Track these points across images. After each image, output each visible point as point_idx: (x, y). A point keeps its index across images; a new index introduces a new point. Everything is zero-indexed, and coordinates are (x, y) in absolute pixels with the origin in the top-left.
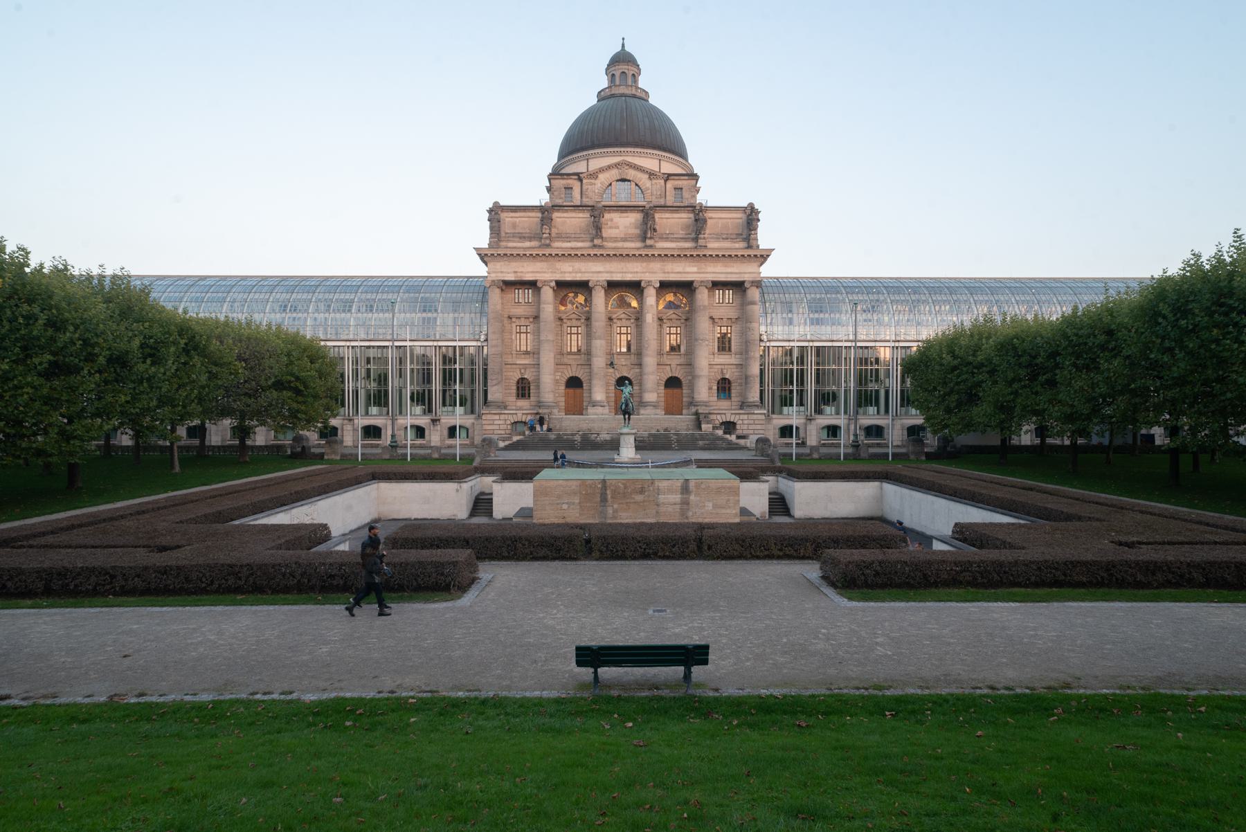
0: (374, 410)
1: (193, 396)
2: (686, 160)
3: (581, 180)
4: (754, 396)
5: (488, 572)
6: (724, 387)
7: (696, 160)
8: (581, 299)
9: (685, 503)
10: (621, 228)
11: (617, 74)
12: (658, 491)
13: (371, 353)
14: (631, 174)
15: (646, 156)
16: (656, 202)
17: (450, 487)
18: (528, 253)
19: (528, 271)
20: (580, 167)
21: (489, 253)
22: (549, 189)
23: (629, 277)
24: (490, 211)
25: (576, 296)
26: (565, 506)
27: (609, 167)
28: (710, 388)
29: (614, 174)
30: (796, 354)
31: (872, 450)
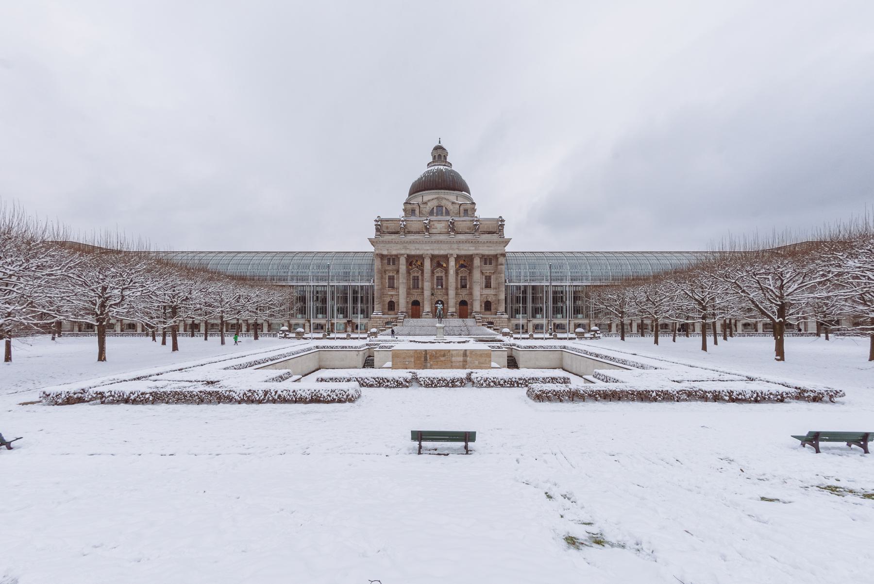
0: (320, 316)
1: (294, 335)
4: (502, 308)
6: (488, 306)
7: (474, 196)
12: (452, 356)
13: (319, 289)
22: (405, 210)
30: (522, 289)
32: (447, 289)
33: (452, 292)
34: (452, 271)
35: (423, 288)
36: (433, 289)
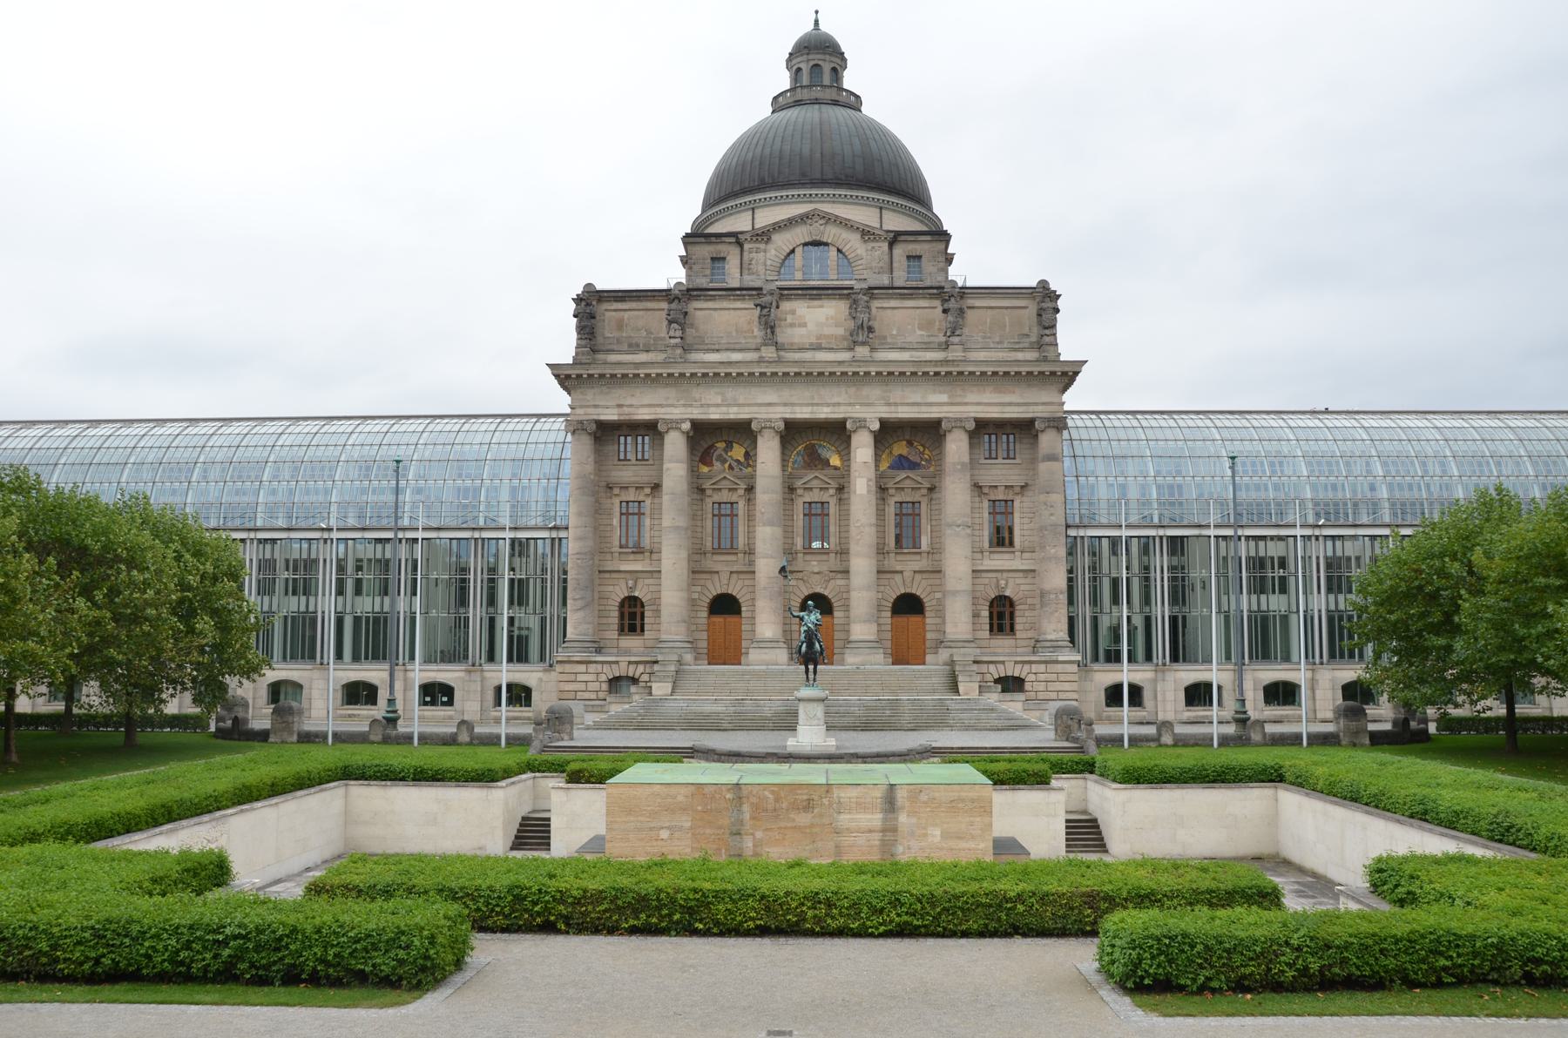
2: (930, 208)
3: (741, 245)
4: (1056, 629)
5: (487, 950)
6: (1001, 615)
7: (944, 208)
8: (738, 452)
9: (890, 830)
10: (811, 326)
11: (805, 67)
14: (830, 233)
15: (856, 202)
16: (874, 280)
17: (471, 795)
18: (642, 372)
19: (642, 405)
20: (740, 223)
21: (573, 372)
22: (685, 261)
23: (824, 413)
24: (578, 300)
25: (729, 446)
26: (664, 834)
27: (790, 223)
28: (976, 615)
29: (800, 234)
31: (1270, 729)
32: (843, 553)
33: (862, 565)
34: (862, 485)
35: (750, 552)
36: (789, 552)
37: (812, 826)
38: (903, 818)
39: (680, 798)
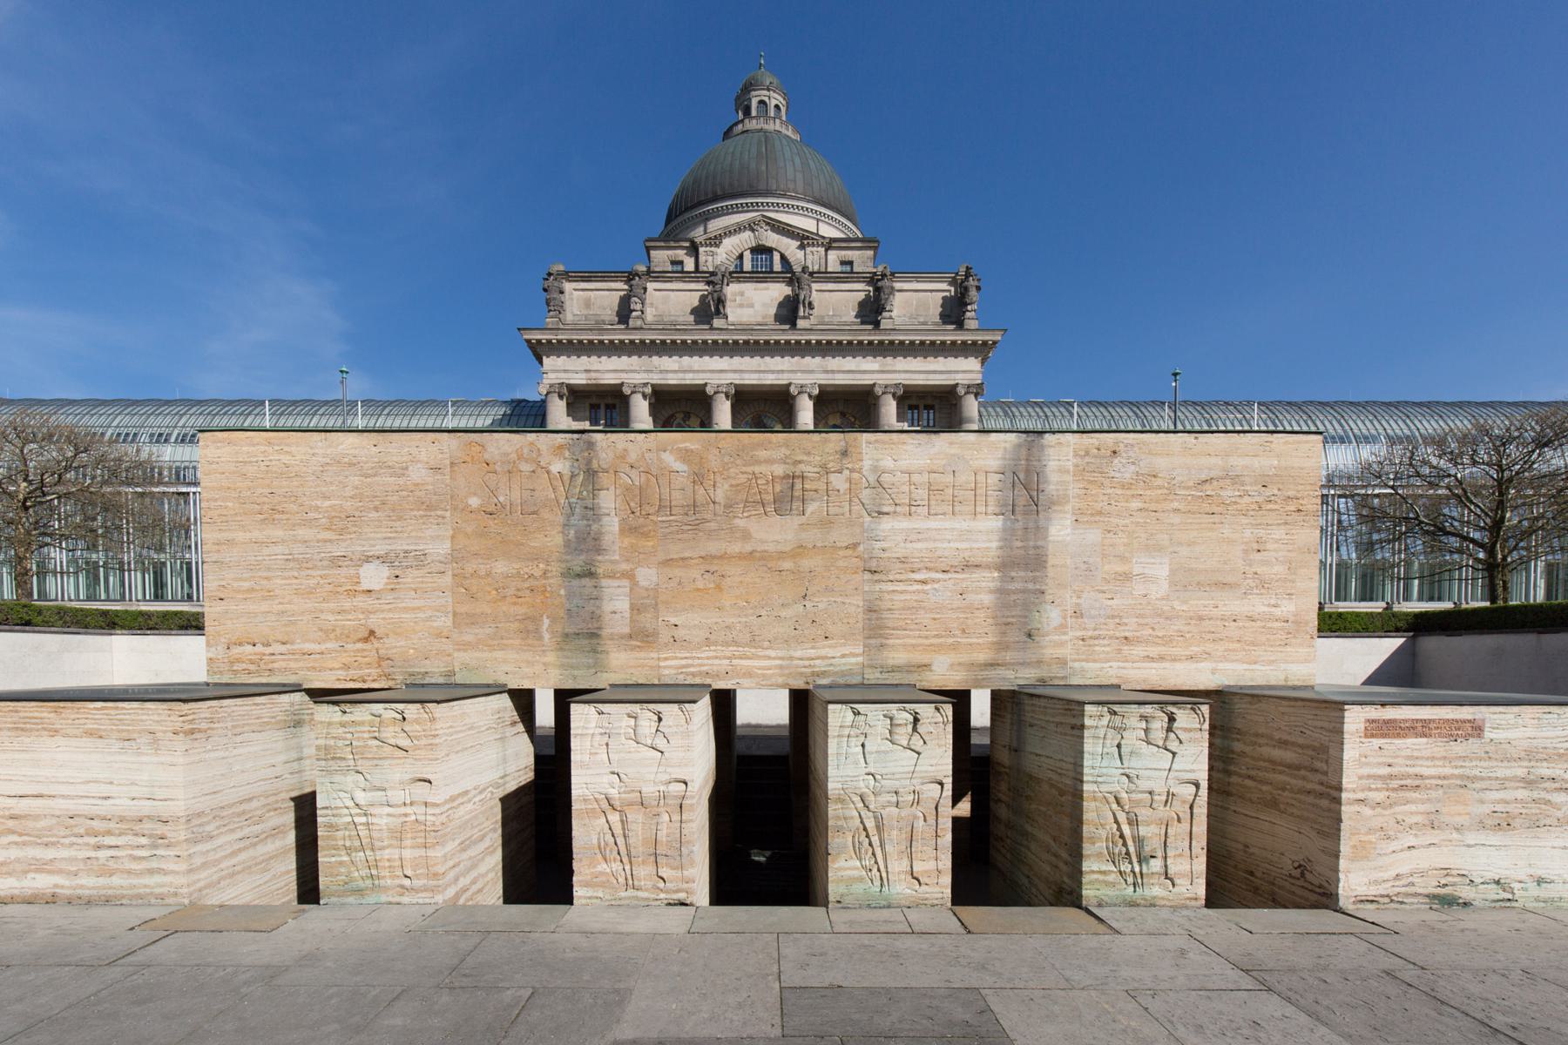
10: (757, 306)
37: (800, 550)
38: (1061, 530)
39: (418, 474)
